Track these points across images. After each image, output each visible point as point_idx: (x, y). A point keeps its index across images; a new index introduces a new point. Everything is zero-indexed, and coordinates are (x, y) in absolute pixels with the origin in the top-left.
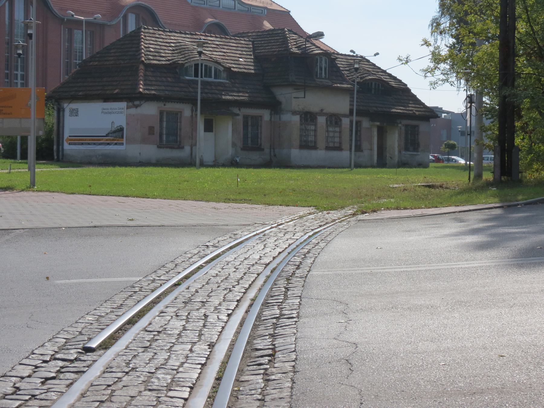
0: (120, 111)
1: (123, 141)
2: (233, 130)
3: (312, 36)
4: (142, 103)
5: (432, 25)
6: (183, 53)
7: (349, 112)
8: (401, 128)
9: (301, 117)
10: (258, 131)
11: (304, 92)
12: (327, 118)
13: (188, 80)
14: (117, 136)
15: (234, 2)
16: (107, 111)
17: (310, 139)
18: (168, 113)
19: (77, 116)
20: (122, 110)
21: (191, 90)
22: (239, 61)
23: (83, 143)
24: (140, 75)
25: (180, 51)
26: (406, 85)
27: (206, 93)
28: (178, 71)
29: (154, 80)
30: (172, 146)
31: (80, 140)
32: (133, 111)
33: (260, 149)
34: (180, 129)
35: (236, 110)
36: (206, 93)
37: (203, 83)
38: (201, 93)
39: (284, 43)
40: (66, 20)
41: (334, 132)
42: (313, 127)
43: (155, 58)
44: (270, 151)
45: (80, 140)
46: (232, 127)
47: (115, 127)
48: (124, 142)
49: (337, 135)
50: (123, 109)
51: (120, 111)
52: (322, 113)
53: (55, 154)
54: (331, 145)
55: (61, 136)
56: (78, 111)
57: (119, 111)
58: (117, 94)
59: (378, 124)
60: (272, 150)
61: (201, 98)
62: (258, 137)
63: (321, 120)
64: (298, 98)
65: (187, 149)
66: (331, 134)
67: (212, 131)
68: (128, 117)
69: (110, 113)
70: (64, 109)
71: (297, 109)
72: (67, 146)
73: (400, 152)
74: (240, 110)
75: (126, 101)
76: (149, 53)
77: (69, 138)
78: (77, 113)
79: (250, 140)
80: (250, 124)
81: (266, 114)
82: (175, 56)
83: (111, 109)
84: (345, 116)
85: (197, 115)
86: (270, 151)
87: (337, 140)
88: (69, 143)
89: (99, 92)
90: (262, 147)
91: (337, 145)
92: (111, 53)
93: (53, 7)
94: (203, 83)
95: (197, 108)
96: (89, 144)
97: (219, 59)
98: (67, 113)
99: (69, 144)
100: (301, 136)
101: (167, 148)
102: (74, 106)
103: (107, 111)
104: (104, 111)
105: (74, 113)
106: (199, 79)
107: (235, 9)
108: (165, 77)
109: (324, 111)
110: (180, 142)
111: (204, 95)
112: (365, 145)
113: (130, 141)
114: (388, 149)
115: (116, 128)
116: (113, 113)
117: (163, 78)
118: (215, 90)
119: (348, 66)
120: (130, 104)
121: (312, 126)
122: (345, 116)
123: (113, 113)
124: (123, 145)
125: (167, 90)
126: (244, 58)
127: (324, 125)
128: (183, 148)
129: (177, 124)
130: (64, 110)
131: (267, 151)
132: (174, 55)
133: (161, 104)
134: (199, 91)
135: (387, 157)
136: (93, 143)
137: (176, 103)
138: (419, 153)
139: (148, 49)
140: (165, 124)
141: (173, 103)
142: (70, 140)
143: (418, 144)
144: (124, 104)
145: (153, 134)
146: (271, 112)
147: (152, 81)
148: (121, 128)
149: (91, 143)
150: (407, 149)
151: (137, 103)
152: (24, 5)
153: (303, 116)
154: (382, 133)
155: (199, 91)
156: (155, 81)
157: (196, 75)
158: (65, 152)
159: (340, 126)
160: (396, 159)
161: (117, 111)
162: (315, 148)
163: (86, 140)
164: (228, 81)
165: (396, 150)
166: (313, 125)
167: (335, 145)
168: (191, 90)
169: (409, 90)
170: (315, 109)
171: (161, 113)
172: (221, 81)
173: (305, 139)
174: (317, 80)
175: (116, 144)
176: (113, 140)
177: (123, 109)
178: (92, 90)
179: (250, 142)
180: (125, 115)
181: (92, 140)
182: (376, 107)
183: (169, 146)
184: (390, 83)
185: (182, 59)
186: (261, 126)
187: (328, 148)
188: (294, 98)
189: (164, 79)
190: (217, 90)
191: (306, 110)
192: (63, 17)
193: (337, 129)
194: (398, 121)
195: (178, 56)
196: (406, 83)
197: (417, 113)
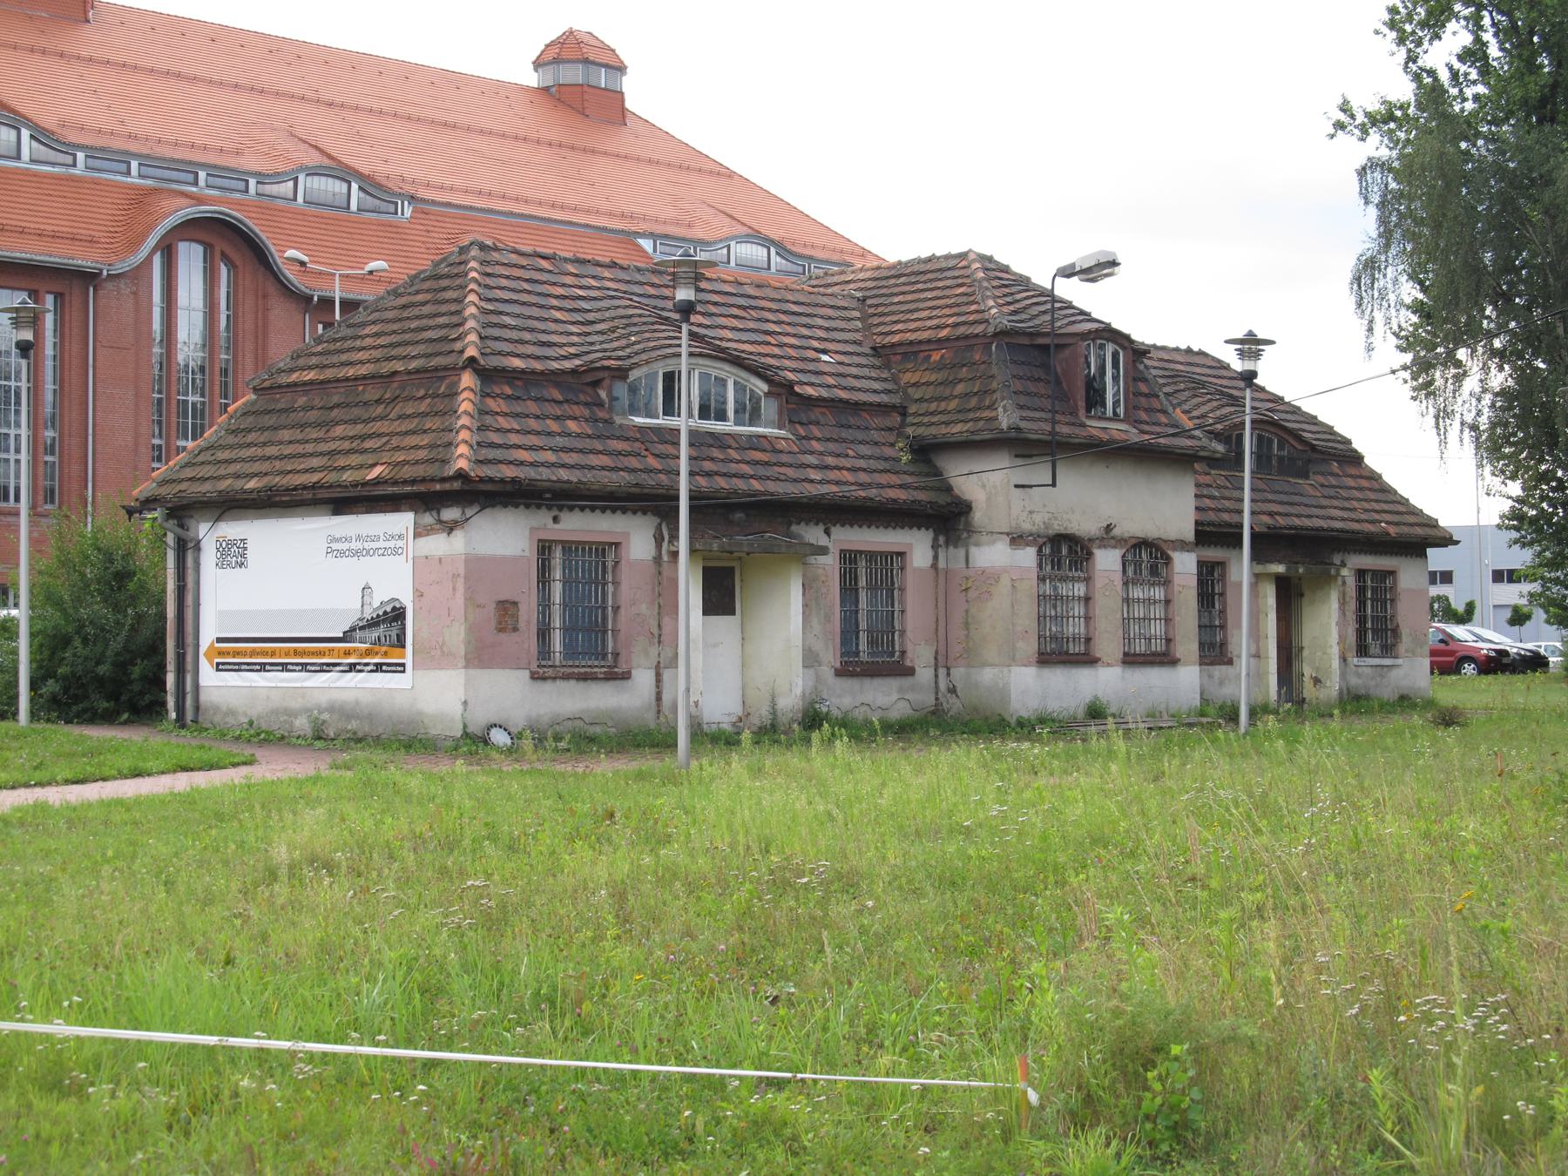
0: (391, 544)
1: (404, 657)
2: (805, 606)
3: (1078, 269)
4: (469, 512)
5: (1358, 279)
6: (623, 331)
7: (1193, 533)
8: (1344, 583)
9: (1040, 551)
10: (893, 606)
11: (1050, 464)
12: (1124, 556)
13: (641, 429)
14: (383, 639)
15: (765, 250)
16: (345, 546)
17: (1071, 629)
18: (568, 546)
19: (241, 565)
20: (400, 543)
21: (653, 462)
22: (818, 360)
23: (265, 664)
24: (461, 409)
25: (611, 324)
26: (1349, 442)
27: (708, 474)
28: (603, 394)
29: (517, 427)
30: (588, 670)
31: (253, 653)
32: (438, 544)
33: (902, 670)
34: (616, 609)
35: (813, 534)
36: (708, 474)
37: (696, 438)
38: (692, 474)
39: (972, 298)
40: (316, 299)
41: (1150, 602)
42: (1080, 589)
43: (521, 349)
44: (936, 676)
45: (253, 653)
46: (804, 594)
47: (376, 604)
48: (408, 661)
49: (1158, 611)
50: (400, 537)
51: (391, 544)
52: (1108, 536)
53: (171, 702)
54: (1140, 647)
55: (189, 640)
56: (245, 549)
57: (387, 544)
58: (378, 482)
59: (1280, 569)
60: (942, 672)
61: (690, 490)
62: (893, 627)
63: (1107, 561)
64: (1031, 487)
65: (643, 678)
66: (1139, 611)
67: (733, 613)
68: (421, 565)
69: (357, 553)
70: (199, 541)
71: (1027, 526)
72: (209, 677)
73: (1344, 659)
74: (827, 532)
75: (411, 509)
76: (496, 332)
77: (217, 645)
78: (243, 556)
79: (863, 637)
80: (862, 582)
81: (918, 547)
82: (592, 344)
83: (359, 538)
84: (1182, 545)
85: (675, 555)
86: (936, 676)
87: (1157, 629)
88: (218, 664)
89: (315, 478)
90: (908, 663)
91: (1157, 646)
92: (363, 338)
93: (280, 265)
94: (696, 438)
95: (677, 529)
96: (284, 667)
97: (751, 353)
98: (209, 556)
99: (218, 670)
100: (1041, 618)
101: (566, 677)
102: (232, 529)
103: (345, 546)
104: (335, 546)
105: (235, 555)
106: (683, 423)
107: (769, 268)
108: (557, 418)
109: (1116, 532)
110: (616, 655)
111: (702, 482)
112: (1241, 643)
113: (431, 657)
114: (1306, 653)
115: (378, 608)
116: (368, 552)
117: (548, 421)
118: (738, 462)
119: (1170, 380)
120: (428, 519)
121: (1076, 585)
122: (1182, 545)
123: (368, 552)
124: (404, 672)
125: (563, 466)
126: (836, 352)
127: (1118, 578)
128: (626, 676)
129: (603, 589)
130: (197, 547)
131: (924, 674)
132: (589, 339)
133: (540, 521)
134: (684, 466)
135: (1306, 679)
136: (297, 664)
137: (598, 511)
138: (1400, 661)
139: (494, 319)
140: (557, 590)
141: (608, 512)
142: (221, 653)
143: (1396, 632)
144: (403, 521)
145: (515, 629)
146: (935, 540)
147: (508, 431)
148: (394, 609)
149: (292, 664)
150: (1362, 650)
151: (450, 514)
152: (205, 261)
153: (1047, 550)
154: (1290, 596)
155: (684, 466)
156: (518, 432)
157: (670, 408)
158: (203, 697)
159: (1167, 583)
160: (1333, 686)
161: (381, 544)
162: (1087, 659)
163: (273, 654)
164: (783, 433)
165: (1335, 651)
166: (1079, 580)
167: (1153, 649)
168: (653, 462)
169: (1356, 459)
170: (1084, 525)
171: (544, 548)
172: (760, 430)
173: (1054, 629)
174: (1089, 423)
175: (378, 668)
176: (368, 653)
177: (400, 537)
178: (290, 472)
179: (863, 646)
180: (410, 561)
181: (296, 653)
182: (1271, 514)
183: (576, 670)
184: (1305, 434)
185: (620, 353)
186: (902, 589)
187: (1131, 660)
188: (1016, 486)
189: (554, 426)
190: (748, 463)
191: (1057, 528)
192: (308, 291)
193: (1158, 593)
194: (1337, 559)
195: (602, 342)
196: (1348, 436)
197: (1392, 530)
